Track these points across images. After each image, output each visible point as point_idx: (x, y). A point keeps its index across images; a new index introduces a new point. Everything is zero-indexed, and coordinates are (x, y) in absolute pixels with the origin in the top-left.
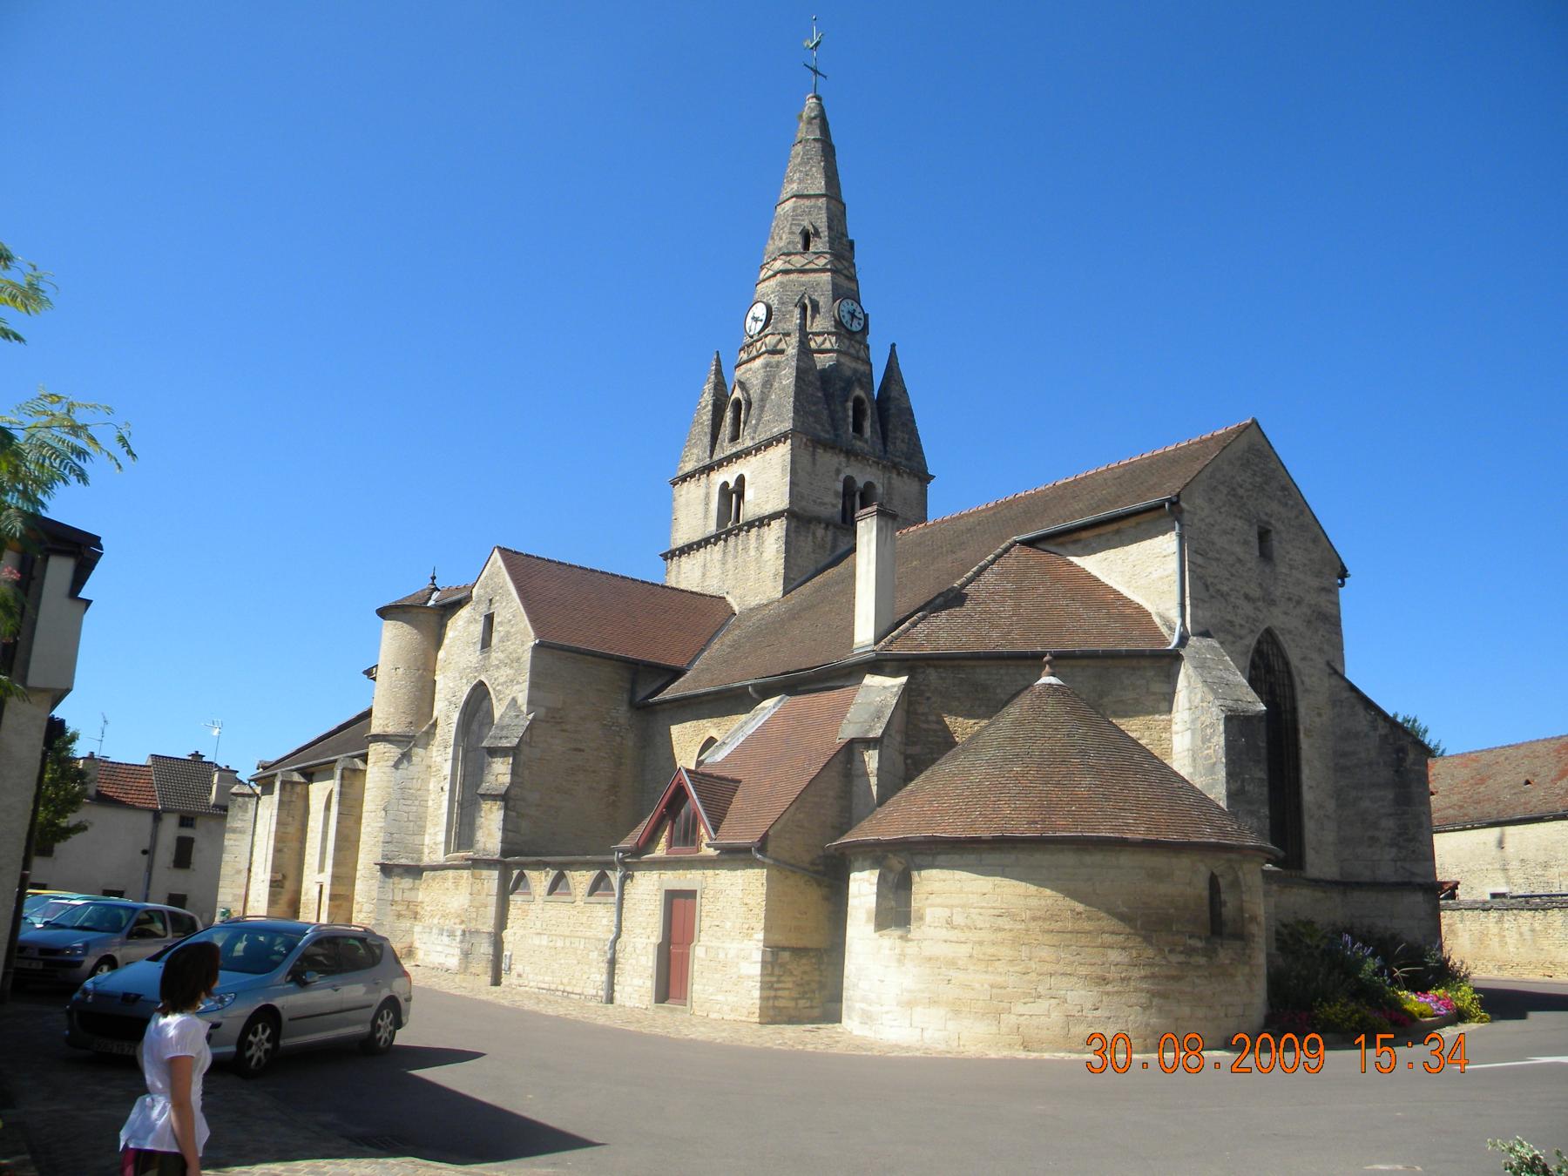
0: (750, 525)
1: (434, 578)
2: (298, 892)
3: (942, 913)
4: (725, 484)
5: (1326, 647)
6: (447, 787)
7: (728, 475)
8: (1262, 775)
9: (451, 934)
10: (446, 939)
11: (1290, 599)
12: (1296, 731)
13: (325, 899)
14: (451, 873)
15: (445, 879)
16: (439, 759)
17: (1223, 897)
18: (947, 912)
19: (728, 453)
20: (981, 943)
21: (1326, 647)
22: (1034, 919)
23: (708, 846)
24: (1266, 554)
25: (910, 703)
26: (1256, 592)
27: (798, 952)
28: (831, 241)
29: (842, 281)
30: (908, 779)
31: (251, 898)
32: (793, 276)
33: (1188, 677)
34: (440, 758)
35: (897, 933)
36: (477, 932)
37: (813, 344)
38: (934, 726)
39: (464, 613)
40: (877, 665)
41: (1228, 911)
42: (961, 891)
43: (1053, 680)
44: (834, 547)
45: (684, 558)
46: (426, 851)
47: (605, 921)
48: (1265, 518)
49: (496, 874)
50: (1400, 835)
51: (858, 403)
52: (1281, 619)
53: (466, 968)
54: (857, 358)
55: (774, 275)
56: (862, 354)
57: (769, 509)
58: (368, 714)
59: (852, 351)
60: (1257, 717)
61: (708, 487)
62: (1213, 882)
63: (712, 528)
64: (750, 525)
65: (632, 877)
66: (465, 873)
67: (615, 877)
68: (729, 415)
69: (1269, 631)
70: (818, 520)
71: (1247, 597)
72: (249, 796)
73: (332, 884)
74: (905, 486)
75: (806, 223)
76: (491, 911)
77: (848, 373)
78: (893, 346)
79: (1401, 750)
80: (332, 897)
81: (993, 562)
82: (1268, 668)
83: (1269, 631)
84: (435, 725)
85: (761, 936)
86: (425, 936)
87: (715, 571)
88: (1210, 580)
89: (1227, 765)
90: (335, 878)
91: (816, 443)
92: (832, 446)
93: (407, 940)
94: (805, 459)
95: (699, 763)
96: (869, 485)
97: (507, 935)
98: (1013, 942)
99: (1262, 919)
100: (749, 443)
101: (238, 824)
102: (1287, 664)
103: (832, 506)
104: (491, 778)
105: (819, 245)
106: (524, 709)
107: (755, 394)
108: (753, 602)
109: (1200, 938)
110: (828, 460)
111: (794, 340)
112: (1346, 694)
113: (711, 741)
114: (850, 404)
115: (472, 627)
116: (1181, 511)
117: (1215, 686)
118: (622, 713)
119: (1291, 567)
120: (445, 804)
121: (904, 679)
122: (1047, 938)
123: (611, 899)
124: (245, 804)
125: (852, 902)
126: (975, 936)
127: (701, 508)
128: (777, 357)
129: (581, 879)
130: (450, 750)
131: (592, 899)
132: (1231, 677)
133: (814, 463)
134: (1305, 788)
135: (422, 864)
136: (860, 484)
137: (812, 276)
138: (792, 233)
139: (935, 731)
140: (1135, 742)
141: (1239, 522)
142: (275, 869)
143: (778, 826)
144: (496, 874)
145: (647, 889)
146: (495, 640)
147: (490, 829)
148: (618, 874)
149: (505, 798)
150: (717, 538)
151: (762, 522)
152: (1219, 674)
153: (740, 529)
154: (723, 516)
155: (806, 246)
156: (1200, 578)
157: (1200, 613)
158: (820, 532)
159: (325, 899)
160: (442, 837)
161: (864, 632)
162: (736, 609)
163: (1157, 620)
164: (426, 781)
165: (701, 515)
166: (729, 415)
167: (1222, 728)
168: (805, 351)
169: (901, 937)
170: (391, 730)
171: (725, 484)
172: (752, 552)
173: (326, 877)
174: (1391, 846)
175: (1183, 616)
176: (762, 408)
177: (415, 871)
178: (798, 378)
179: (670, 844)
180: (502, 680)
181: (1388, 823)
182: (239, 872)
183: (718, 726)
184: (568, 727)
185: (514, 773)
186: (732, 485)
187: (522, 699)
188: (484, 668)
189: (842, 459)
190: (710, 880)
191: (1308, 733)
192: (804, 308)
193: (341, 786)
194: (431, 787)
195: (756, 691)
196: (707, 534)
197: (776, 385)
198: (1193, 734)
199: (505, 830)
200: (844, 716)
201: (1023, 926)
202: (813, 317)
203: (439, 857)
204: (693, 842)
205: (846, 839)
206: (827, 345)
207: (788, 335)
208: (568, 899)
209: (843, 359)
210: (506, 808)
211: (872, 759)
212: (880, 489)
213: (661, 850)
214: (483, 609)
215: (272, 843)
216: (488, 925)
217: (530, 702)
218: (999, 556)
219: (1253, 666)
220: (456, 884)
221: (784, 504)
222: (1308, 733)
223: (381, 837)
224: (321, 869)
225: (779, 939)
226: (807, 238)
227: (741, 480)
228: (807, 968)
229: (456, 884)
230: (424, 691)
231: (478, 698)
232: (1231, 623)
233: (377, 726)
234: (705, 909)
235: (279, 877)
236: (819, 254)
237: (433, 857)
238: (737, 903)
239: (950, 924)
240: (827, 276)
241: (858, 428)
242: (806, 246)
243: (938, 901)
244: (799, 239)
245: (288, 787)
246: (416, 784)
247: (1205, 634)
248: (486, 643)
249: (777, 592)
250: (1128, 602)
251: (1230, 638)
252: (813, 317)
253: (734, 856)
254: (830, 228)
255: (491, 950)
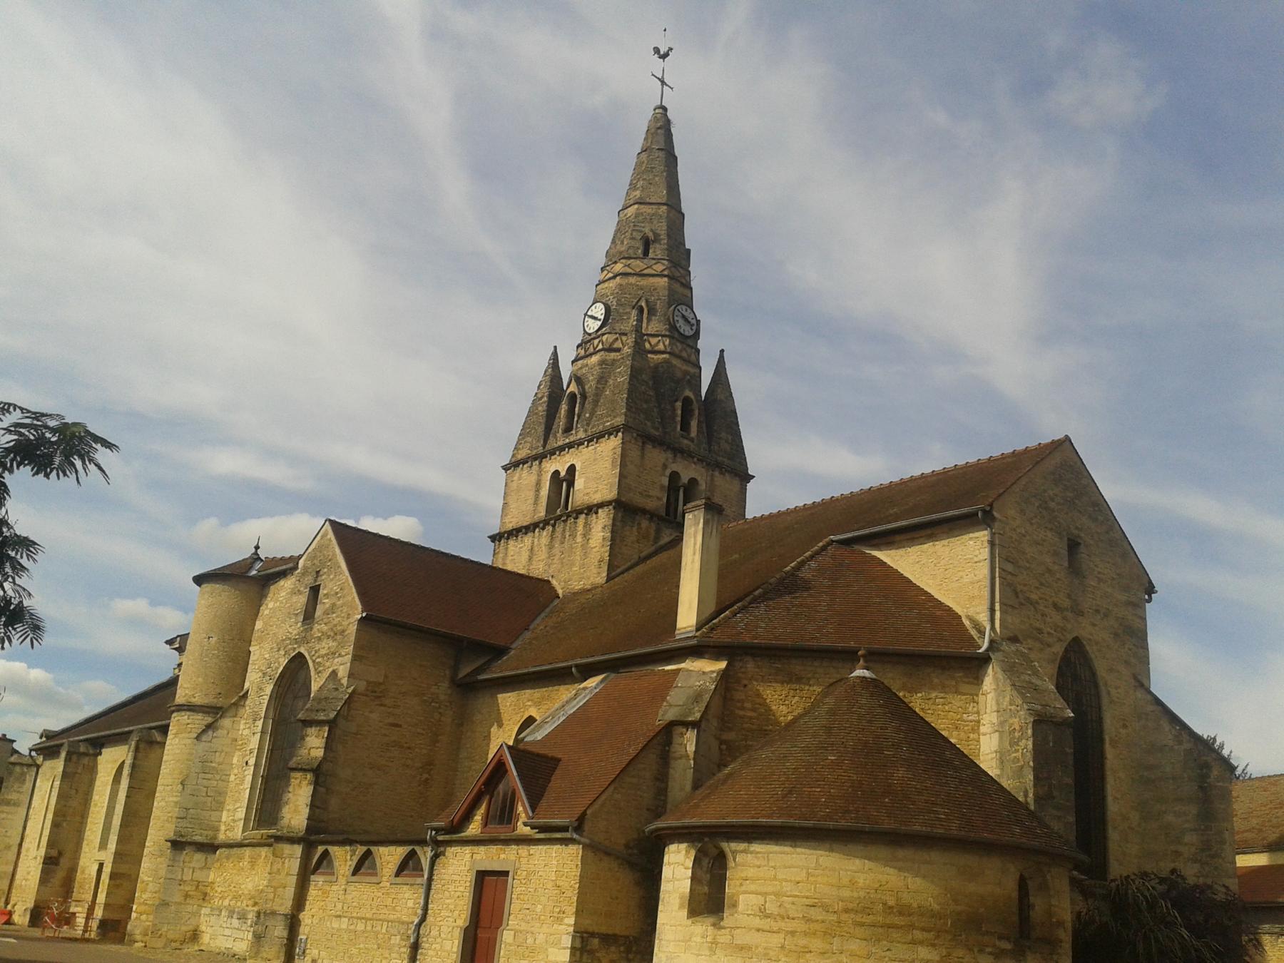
0: (578, 512)
1: (257, 548)
2: (73, 870)
3: (756, 900)
4: (557, 473)
5: (1133, 660)
6: (252, 761)
7: (559, 464)
8: (1069, 781)
9: (242, 917)
10: (235, 922)
11: (1097, 611)
12: (1102, 740)
13: (105, 877)
14: (248, 852)
15: (241, 859)
16: (246, 732)
17: (1032, 899)
18: (761, 899)
19: (560, 443)
20: (793, 933)
21: (1133, 660)
22: (846, 911)
23: (525, 824)
24: (1074, 568)
25: (727, 689)
26: (1066, 603)
27: (607, 939)
28: (670, 249)
29: (677, 286)
30: (722, 765)
31: (18, 876)
32: (632, 280)
33: (996, 679)
34: (248, 733)
35: (711, 920)
36: (273, 913)
37: (647, 346)
38: (750, 714)
39: (287, 584)
40: (696, 651)
41: (1037, 913)
42: (775, 878)
43: (866, 673)
44: (657, 539)
45: (511, 542)
46: (223, 828)
47: (410, 904)
48: (1076, 532)
49: (298, 850)
50: (1203, 850)
51: (687, 402)
52: (1093, 632)
53: (257, 953)
54: (687, 361)
55: (614, 277)
56: (693, 358)
57: (597, 498)
58: (172, 683)
59: (684, 354)
60: (1065, 722)
61: (540, 474)
62: (1022, 884)
63: (542, 513)
64: (578, 512)
65: (443, 854)
66: (264, 851)
67: (425, 855)
68: (564, 407)
69: (1076, 641)
70: (644, 511)
71: (1055, 606)
72: (29, 766)
73: (114, 862)
74: (725, 484)
75: (647, 230)
76: (290, 892)
77: (679, 375)
78: (722, 351)
79: (1206, 766)
80: (113, 876)
81: (812, 557)
82: (1075, 673)
83: (1076, 641)
84: (245, 696)
85: (572, 921)
86: (213, 919)
87: (542, 554)
88: (1019, 588)
89: (1035, 769)
90: (118, 855)
91: (646, 439)
92: (660, 443)
93: (193, 921)
94: (634, 453)
95: (516, 740)
96: (693, 481)
97: (306, 917)
98: (825, 933)
99: (1069, 925)
100: (581, 435)
101: (13, 796)
102: (1094, 674)
103: (656, 500)
104: (303, 752)
105: (657, 251)
106: (345, 681)
107: (590, 386)
108: (577, 586)
109: (1008, 939)
110: (657, 456)
111: (630, 340)
112: (1150, 708)
113: (530, 721)
114: (679, 404)
115: (295, 599)
116: (994, 519)
117: (1025, 690)
118: (443, 690)
119: (1100, 580)
120: (249, 778)
121: (722, 665)
122: (859, 932)
123: (419, 880)
124: (23, 774)
125: (664, 886)
126: (791, 926)
127: (532, 494)
128: (613, 355)
129: (389, 857)
130: (260, 723)
131: (399, 880)
132: (1039, 682)
133: (643, 456)
134: (1110, 799)
135: (216, 842)
136: (685, 479)
137: (652, 280)
138: (633, 239)
139: (751, 718)
140: (946, 740)
141: (1049, 534)
142: (51, 844)
143: (596, 806)
144: (298, 850)
145: (458, 868)
146: (319, 613)
147: (297, 808)
148: (429, 854)
149: (320, 774)
150: (545, 523)
151: (591, 509)
152: (1027, 678)
153: (569, 516)
154: (553, 503)
155: (646, 253)
156: (1010, 585)
157: (1009, 619)
158: (645, 523)
159: (105, 877)
160: (241, 814)
161: (687, 618)
162: (560, 592)
163: (967, 623)
164: (230, 755)
165: (531, 501)
166: (564, 407)
167: (1030, 732)
168: (639, 350)
169: (714, 925)
170: (198, 700)
171: (557, 473)
172: (579, 539)
173: (108, 857)
174: (1195, 861)
175: (992, 620)
176: (596, 402)
177: (210, 848)
178: (632, 377)
179: (486, 823)
180: (323, 652)
181: (1191, 838)
182: (8, 847)
183: (537, 704)
184: (387, 702)
185: (327, 747)
186: (563, 474)
187: (343, 672)
188: (304, 640)
189: (670, 455)
190: (524, 861)
191: (1114, 743)
192: (641, 310)
193: (135, 758)
194: (235, 760)
195: (578, 671)
196: (536, 519)
197: (611, 382)
198: (1001, 738)
199: (313, 806)
200: (664, 699)
201: (834, 917)
202: (649, 320)
203: (237, 834)
204: (509, 822)
205: (660, 824)
206: (661, 347)
207: (625, 334)
208: (374, 879)
209: (675, 362)
210: (316, 784)
211: (689, 742)
212: (703, 486)
213: (474, 828)
214: (309, 580)
215: (50, 816)
216: (285, 906)
217: (351, 675)
218: (817, 553)
219: (1061, 673)
220: (253, 863)
221: (611, 494)
222: (1114, 743)
223: (176, 812)
224: (103, 845)
225: (589, 924)
226: (647, 243)
227: (572, 469)
228: (615, 957)
229: (253, 863)
230: (237, 662)
231: (294, 675)
232: (1040, 631)
233: (180, 697)
234: (517, 891)
235: (54, 853)
236: (658, 261)
237: (230, 834)
238: (550, 885)
239: (763, 913)
240: (664, 281)
241: (685, 426)
242: (646, 253)
243: (753, 887)
244: (639, 245)
245: (74, 758)
246: (218, 758)
247: (1014, 639)
248: (309, 615)
249: (601, 578)
250: (939, 604)
251: (1038, 645)
252: (649, 320)
253: (549, 833)
254: (669, 236)
255: (285, 934)
